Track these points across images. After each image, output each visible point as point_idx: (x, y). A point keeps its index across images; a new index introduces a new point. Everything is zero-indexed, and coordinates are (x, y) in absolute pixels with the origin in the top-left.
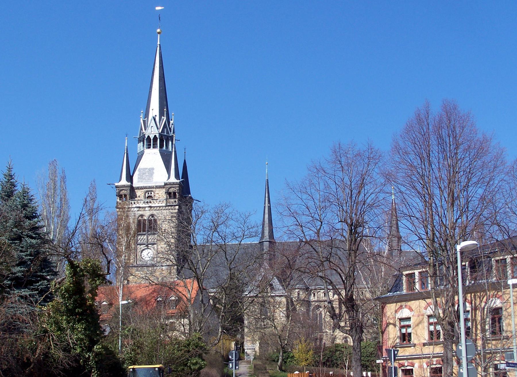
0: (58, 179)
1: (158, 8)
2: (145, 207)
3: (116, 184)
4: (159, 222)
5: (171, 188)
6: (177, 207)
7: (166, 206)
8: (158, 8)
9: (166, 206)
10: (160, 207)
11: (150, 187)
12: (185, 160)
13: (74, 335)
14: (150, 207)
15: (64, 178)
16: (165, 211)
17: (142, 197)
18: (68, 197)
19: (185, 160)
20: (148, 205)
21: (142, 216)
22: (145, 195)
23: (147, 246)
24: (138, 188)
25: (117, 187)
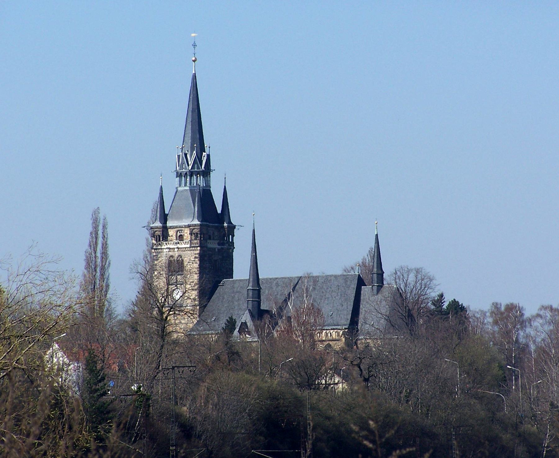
0: (100, 228)
1: (193, 35)
2: (174, 248)
3: (151, 225)
4: (185, 264)
5: (194, 229)
6: (199, 248)
7: (190, 247)
8: (193, 35)
9: (190, 247)
10: (185, 248)
11: (180, 227)
12: (225, 186)
13: (501, 372)
14: (178, 248)
15: (104, 227)
16: (188, 252)
17: (174, 237)
18: (108, 242)
19: (225, 186)
20: (176, 247)
21: (172, 256)
22: (177, 234)
23: (176, 286)
24: (171, 228)
25: (152, 228)
